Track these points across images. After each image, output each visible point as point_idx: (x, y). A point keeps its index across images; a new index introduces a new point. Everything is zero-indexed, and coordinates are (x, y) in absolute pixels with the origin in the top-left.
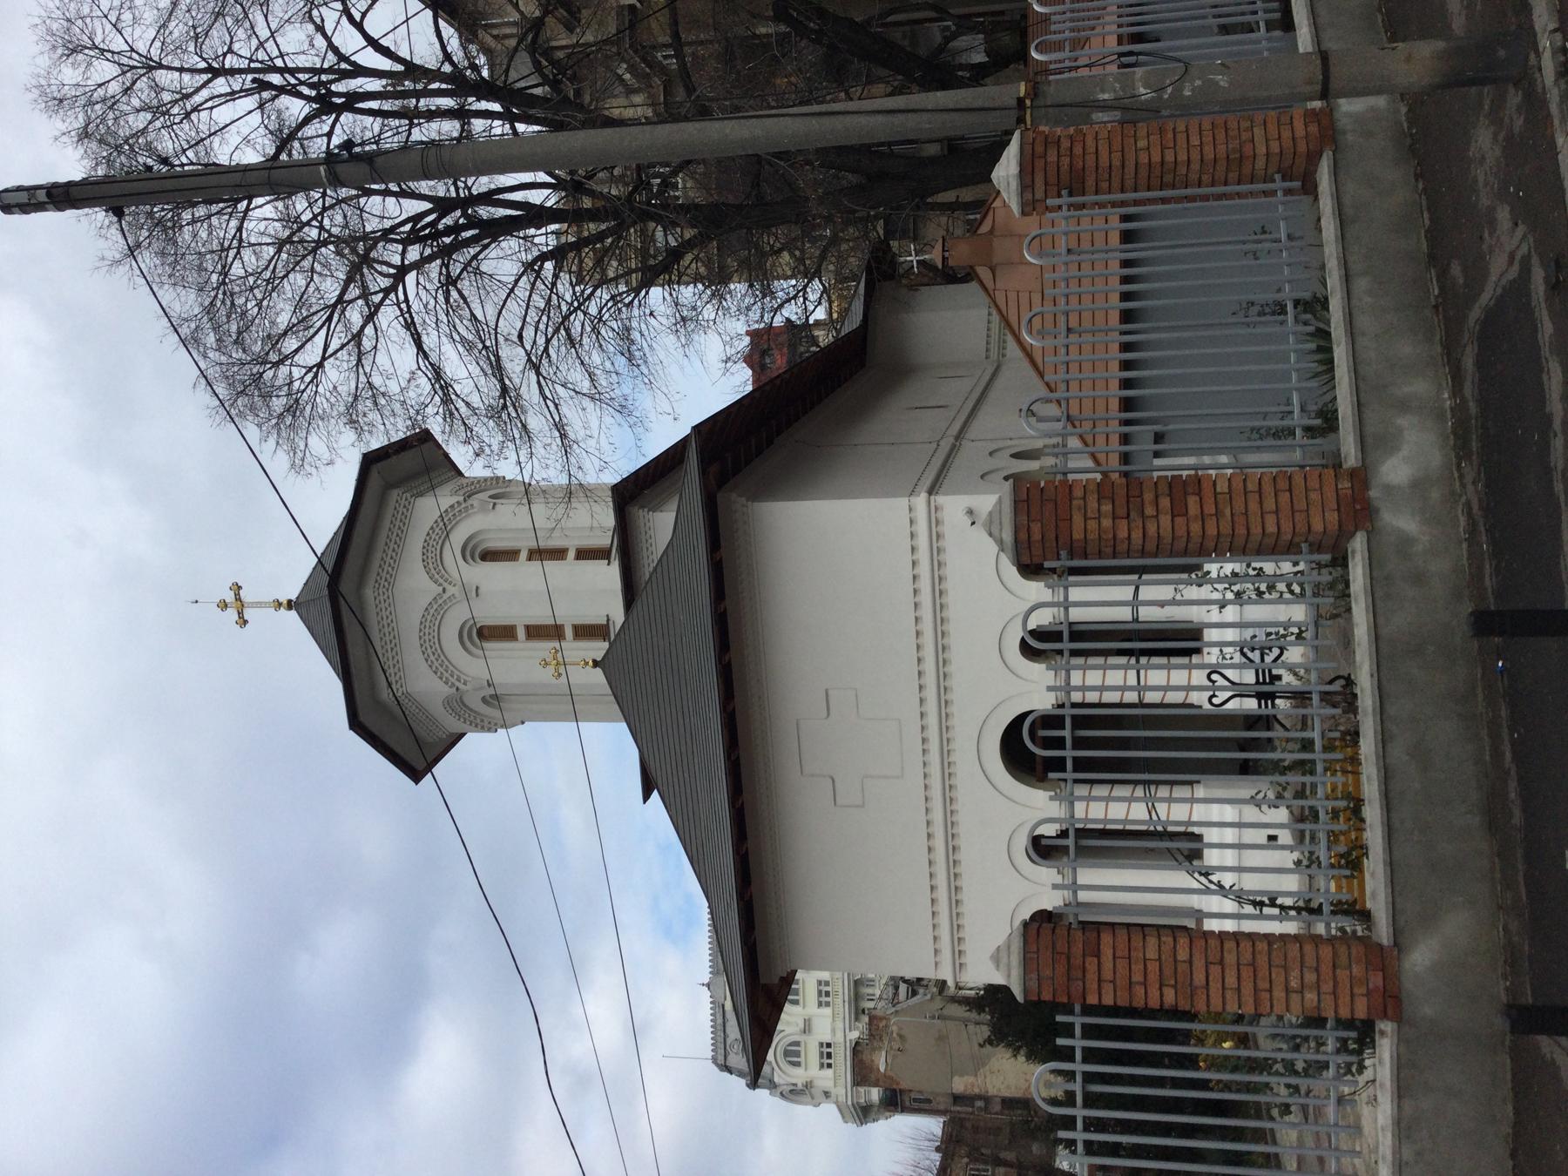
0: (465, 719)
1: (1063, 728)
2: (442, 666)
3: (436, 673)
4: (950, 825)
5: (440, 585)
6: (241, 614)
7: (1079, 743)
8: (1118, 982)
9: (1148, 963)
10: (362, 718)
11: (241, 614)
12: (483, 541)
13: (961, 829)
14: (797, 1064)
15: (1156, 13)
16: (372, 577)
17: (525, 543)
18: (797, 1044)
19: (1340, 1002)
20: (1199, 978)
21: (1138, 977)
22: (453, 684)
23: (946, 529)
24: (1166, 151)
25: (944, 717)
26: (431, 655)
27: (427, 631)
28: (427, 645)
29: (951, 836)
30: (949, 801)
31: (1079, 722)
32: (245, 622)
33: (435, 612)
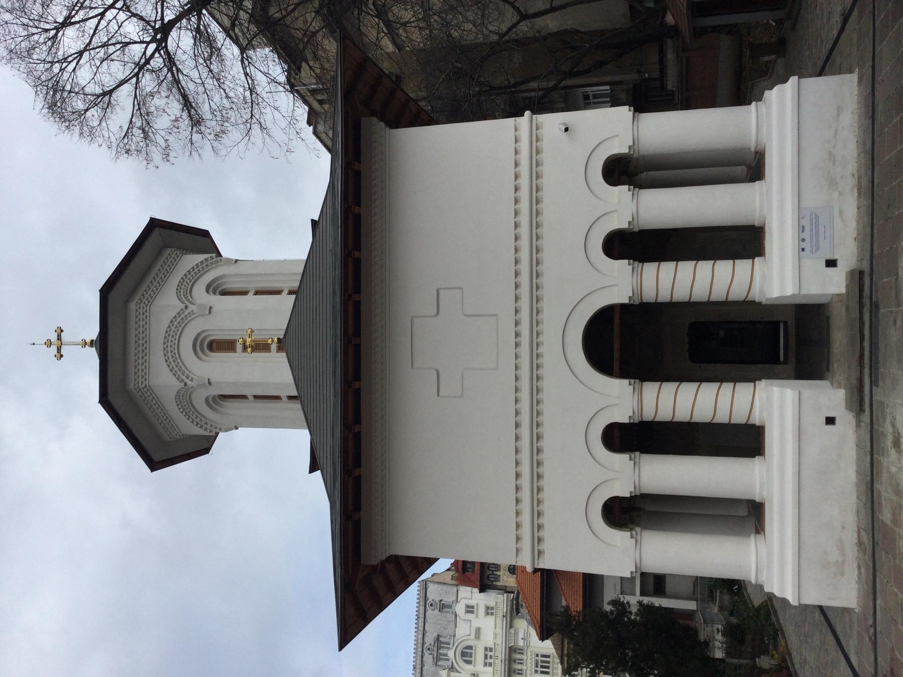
0: (189, 416)
2: (177, 366)
3: (171, 371)
4: (536, 413)
5: (183, 303)
6: (59, 350)
10: (111, 397)
11: (59, 350)
12: (222, 284)
13: (545, 418)
14: (469, 662)
16: (139, 295)
17: (251, 296)
18: (470, 647)
22: (183, 381)
23: (545, 145)
25: (536, 312)
26: (175, 367)
27: (169, 344)
28: (169, 349)
29: (536, 425)
30: (536, 390)
32: (62, 356)
33: (179, 323)
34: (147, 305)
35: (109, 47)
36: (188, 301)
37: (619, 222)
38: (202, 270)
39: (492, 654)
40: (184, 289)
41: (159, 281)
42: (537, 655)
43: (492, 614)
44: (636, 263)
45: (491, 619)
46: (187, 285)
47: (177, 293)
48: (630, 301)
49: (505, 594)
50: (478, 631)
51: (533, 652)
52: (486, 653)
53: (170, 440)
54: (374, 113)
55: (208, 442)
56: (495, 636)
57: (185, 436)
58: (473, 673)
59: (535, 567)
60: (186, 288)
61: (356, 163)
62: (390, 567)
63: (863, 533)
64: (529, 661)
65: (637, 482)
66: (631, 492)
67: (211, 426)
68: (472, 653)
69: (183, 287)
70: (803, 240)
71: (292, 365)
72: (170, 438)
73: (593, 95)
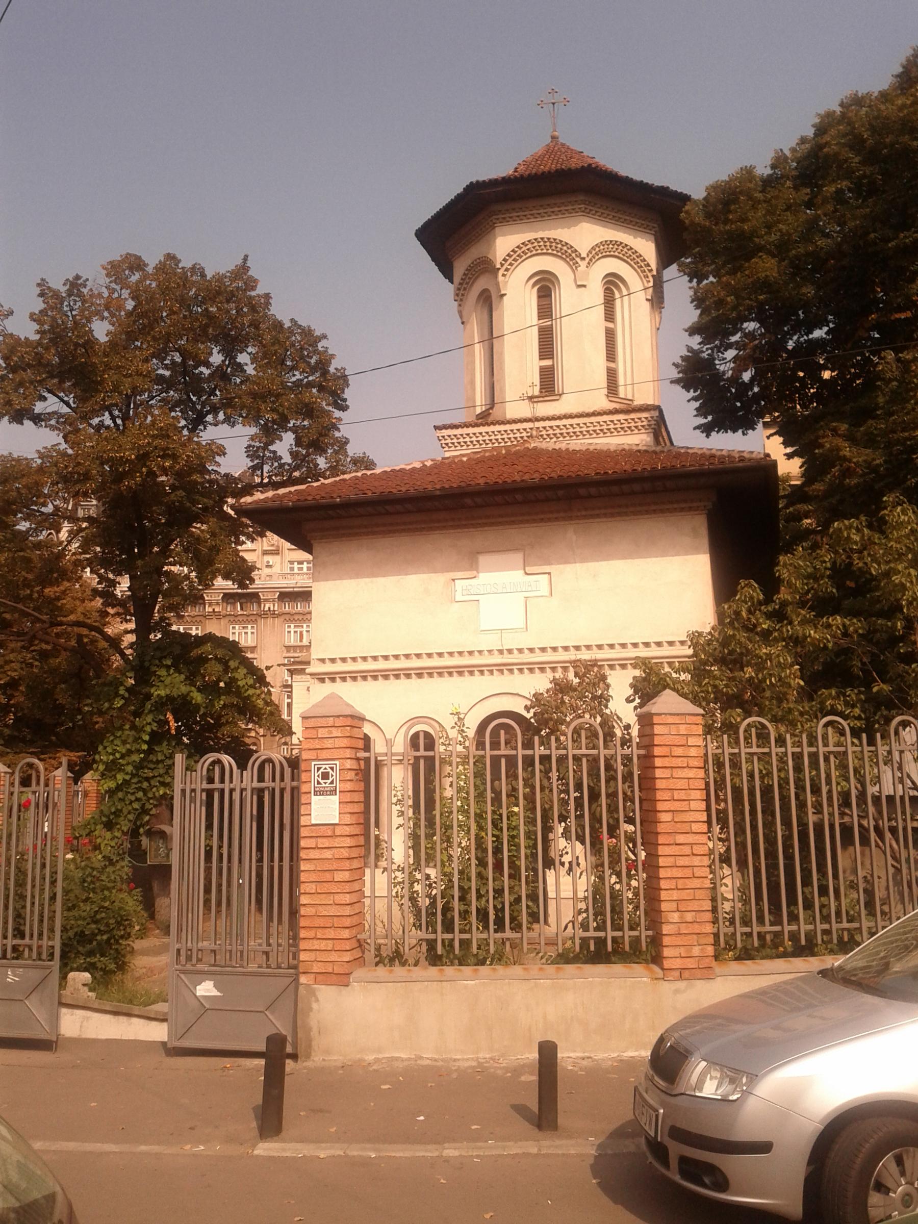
1: (425, 750)
7: (496, 760)
8: (671, 780)
9: (687, 802)
15: (240, 862)
19: (674, 938)
20: (681, 839)
21: (677, 795)
22: (502, 265)
24: (689, 847)
31: (295, 791)
33: (568, 254)
36: (591, 260)
67: (463, 295)
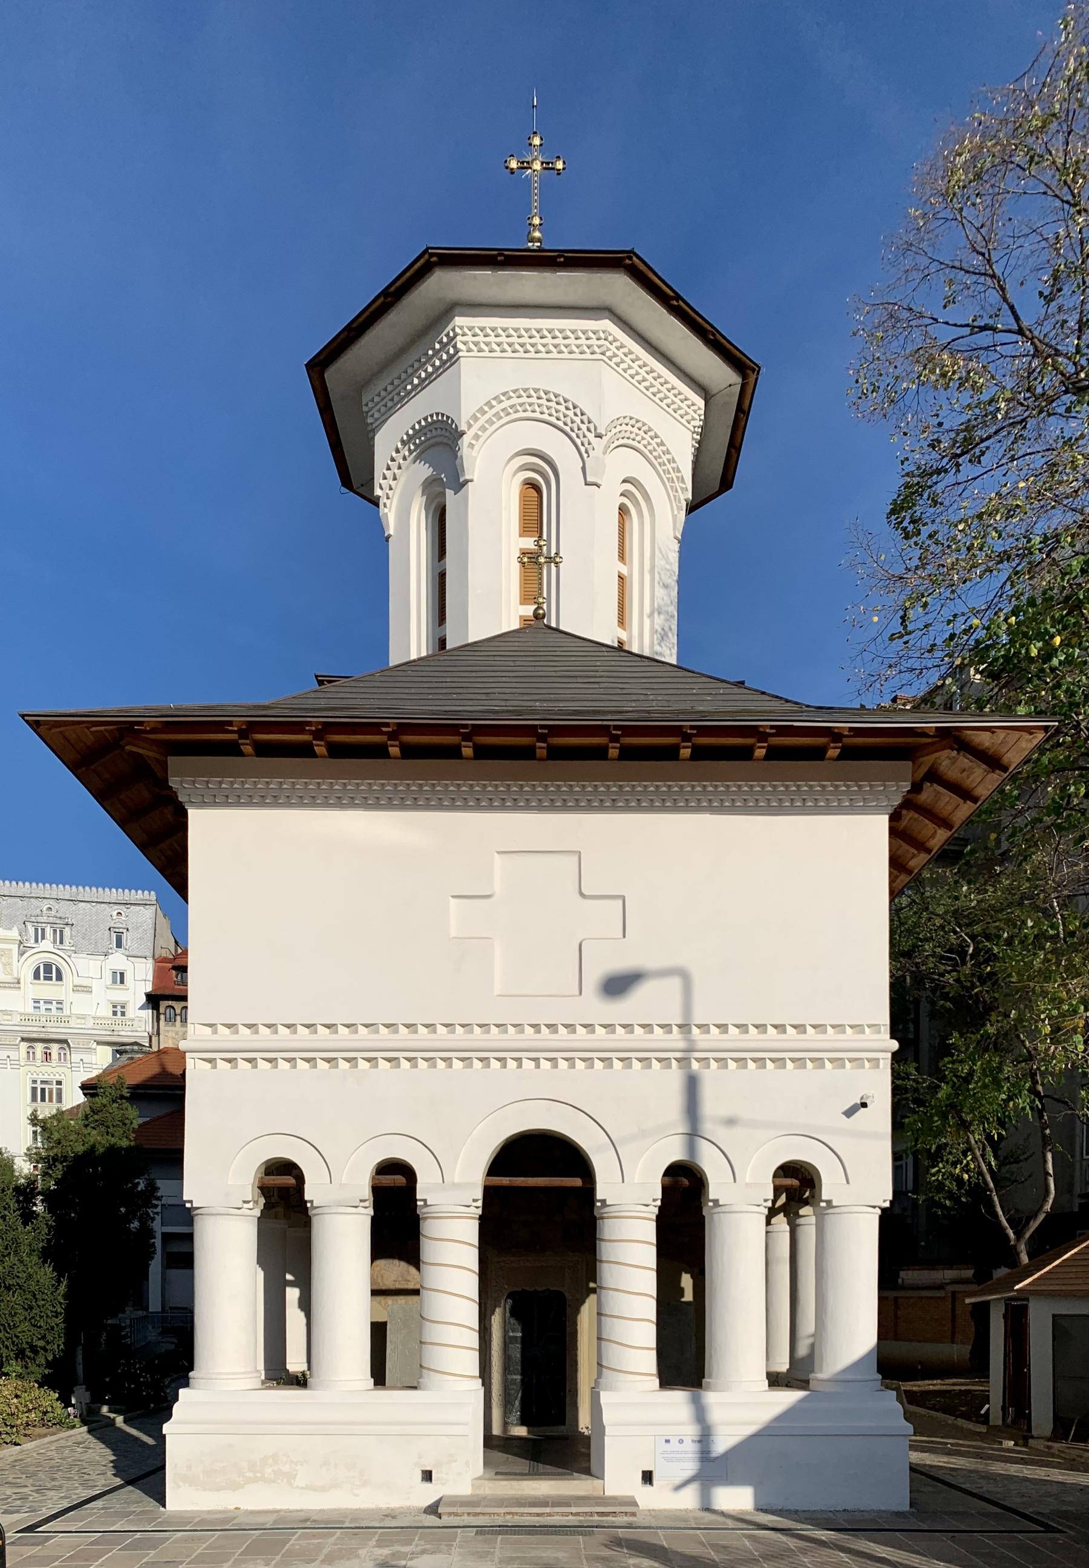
14: (37, 976)
18: (59, 977)
34: (603, 354)
35: (698, 1018)
37: (718, 1187)
38: (664, 471)
39: (54, 1011)
40: (631, 433)
41: (647, 380)
42: (59, 1083)
43: (115, 1013)
44: (656, 1211)
45: (106, 1011)
46: (638, 438)
47: (624, 418)
48: (600, 1201)
49: (146, 1034)
50: (87, 990)
51: (63, 1076)
52: (54, 1002)
53: (364, 403)
54: (917, 788)
55: (362, 485)
56: (83, 1017)
57: (371, 435)
58: (22, 981)
59: (187, 1054)
60: (633, 436)
61: (839, 750)
62: (168, 811)
63: (274, 1517)
64: (49, 1070)
65: (326, 1210)
66: (312, 1202)
68: (52, 980)
69: (635, 430)
70: (681, 1441)
71: (498, 639)
72: (367, 405)
73: (902, 1166)
